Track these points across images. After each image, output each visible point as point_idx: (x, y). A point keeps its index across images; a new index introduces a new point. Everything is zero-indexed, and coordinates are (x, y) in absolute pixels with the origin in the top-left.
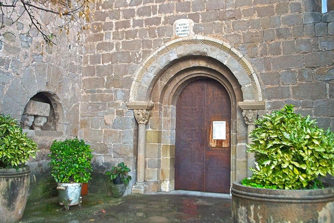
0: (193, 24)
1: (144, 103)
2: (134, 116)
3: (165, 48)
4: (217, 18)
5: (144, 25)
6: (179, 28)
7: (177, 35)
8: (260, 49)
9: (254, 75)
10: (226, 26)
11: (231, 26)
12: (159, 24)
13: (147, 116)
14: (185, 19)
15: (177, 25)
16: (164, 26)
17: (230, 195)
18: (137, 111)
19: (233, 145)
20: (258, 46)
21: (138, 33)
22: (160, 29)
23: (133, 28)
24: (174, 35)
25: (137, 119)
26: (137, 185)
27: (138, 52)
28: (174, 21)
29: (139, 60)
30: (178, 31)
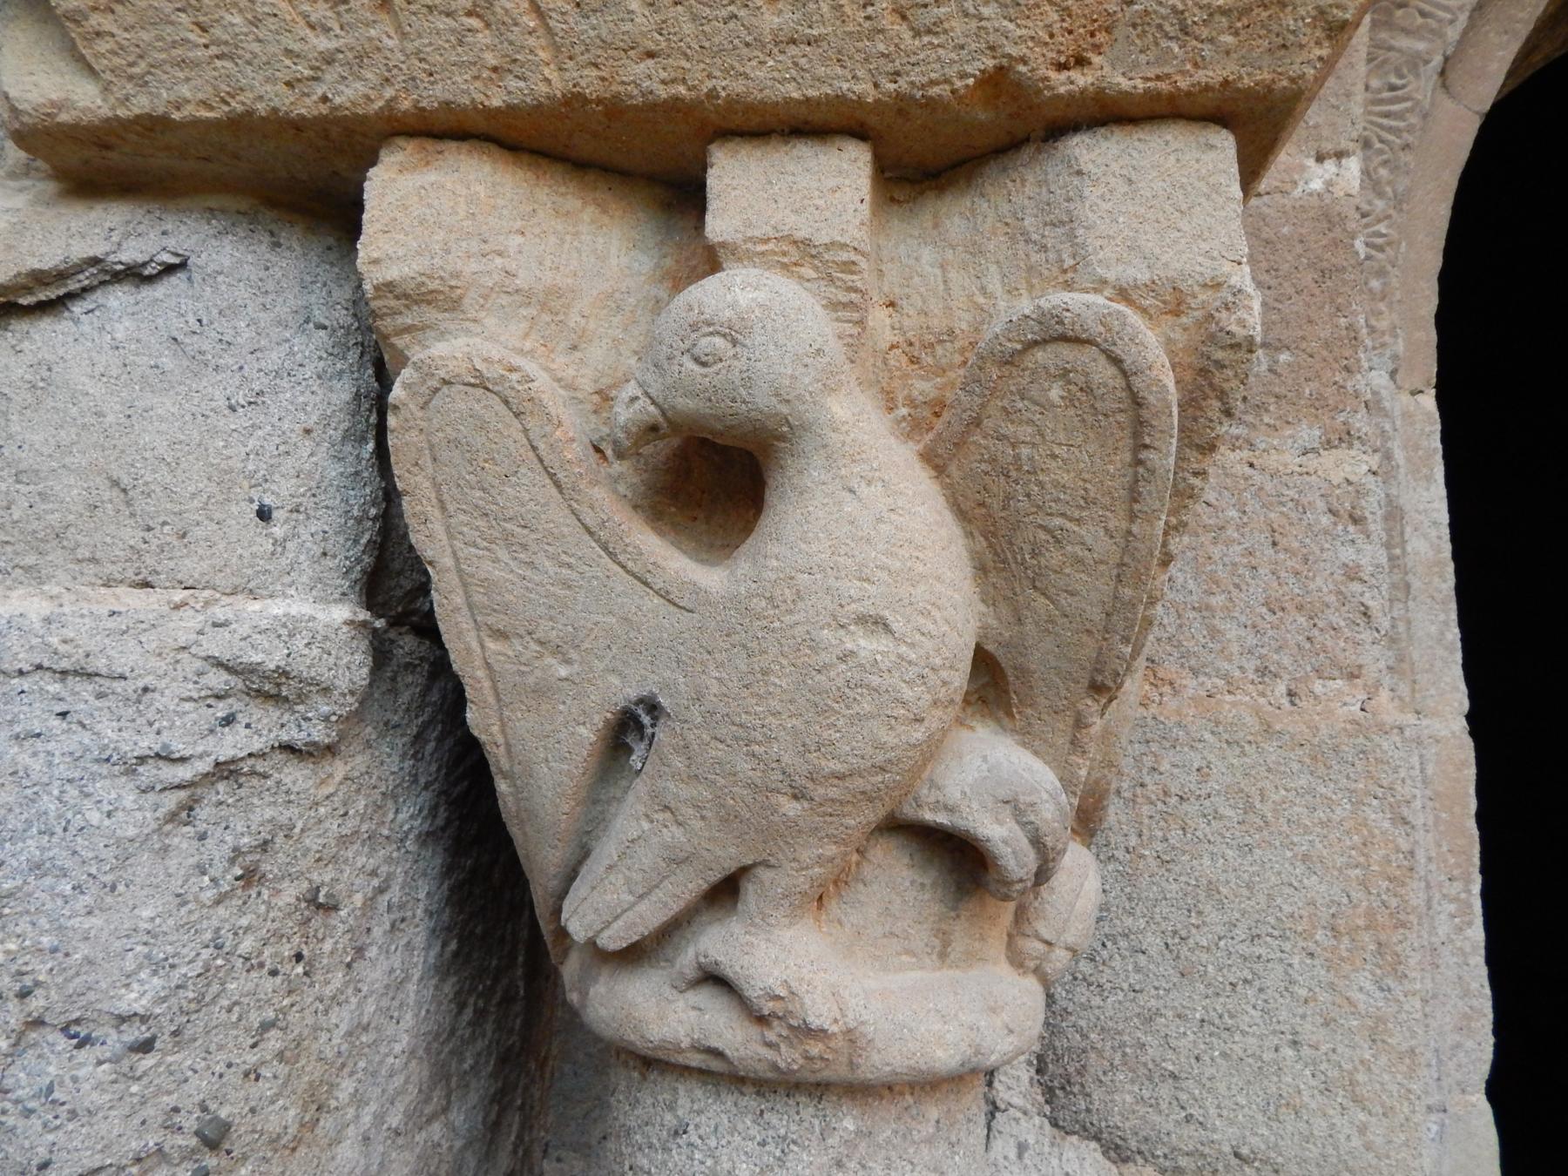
2: (393, 585)
25: (539, 752)
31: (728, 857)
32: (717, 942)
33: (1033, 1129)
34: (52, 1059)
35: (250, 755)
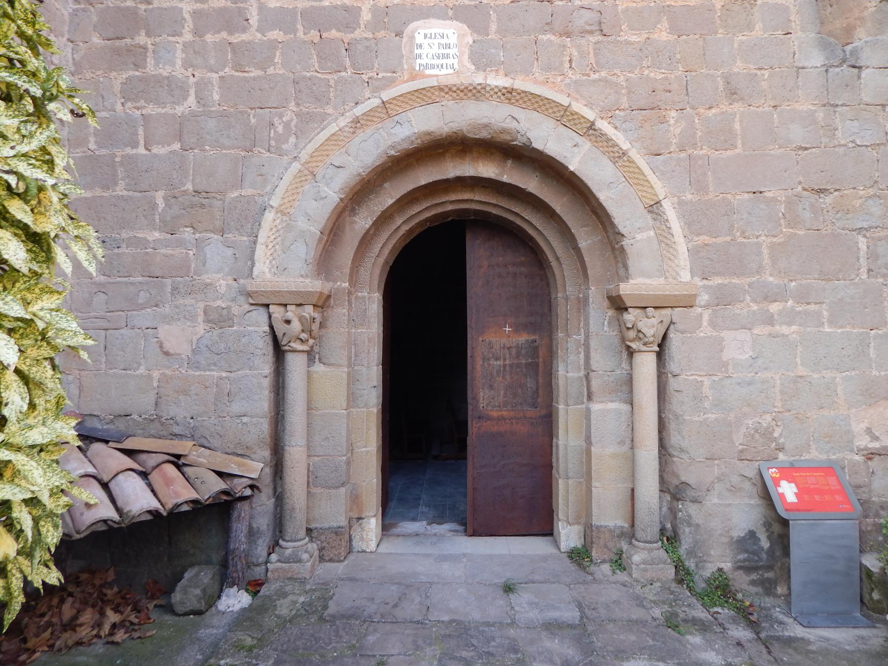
3: (378, 107)
4: (547, 28)
5: (299, 26)
6: (425, 46)
7: (417, 68)
8: (678, 131)
11: (592, 55)
12: (355, 29)
13: (315, 327)
15: (416, 34)
16: (371, 36)
18: (282, 309)
20: (672, 122)
21: (278, 54)
22: (359, 47)
23: (259, 36)
24: (406, 67)
25: (279, 335)
26: (288, 552)
27: (281, 116)
28: (406, 24)
29: (283, 143)
30: (420, 56)
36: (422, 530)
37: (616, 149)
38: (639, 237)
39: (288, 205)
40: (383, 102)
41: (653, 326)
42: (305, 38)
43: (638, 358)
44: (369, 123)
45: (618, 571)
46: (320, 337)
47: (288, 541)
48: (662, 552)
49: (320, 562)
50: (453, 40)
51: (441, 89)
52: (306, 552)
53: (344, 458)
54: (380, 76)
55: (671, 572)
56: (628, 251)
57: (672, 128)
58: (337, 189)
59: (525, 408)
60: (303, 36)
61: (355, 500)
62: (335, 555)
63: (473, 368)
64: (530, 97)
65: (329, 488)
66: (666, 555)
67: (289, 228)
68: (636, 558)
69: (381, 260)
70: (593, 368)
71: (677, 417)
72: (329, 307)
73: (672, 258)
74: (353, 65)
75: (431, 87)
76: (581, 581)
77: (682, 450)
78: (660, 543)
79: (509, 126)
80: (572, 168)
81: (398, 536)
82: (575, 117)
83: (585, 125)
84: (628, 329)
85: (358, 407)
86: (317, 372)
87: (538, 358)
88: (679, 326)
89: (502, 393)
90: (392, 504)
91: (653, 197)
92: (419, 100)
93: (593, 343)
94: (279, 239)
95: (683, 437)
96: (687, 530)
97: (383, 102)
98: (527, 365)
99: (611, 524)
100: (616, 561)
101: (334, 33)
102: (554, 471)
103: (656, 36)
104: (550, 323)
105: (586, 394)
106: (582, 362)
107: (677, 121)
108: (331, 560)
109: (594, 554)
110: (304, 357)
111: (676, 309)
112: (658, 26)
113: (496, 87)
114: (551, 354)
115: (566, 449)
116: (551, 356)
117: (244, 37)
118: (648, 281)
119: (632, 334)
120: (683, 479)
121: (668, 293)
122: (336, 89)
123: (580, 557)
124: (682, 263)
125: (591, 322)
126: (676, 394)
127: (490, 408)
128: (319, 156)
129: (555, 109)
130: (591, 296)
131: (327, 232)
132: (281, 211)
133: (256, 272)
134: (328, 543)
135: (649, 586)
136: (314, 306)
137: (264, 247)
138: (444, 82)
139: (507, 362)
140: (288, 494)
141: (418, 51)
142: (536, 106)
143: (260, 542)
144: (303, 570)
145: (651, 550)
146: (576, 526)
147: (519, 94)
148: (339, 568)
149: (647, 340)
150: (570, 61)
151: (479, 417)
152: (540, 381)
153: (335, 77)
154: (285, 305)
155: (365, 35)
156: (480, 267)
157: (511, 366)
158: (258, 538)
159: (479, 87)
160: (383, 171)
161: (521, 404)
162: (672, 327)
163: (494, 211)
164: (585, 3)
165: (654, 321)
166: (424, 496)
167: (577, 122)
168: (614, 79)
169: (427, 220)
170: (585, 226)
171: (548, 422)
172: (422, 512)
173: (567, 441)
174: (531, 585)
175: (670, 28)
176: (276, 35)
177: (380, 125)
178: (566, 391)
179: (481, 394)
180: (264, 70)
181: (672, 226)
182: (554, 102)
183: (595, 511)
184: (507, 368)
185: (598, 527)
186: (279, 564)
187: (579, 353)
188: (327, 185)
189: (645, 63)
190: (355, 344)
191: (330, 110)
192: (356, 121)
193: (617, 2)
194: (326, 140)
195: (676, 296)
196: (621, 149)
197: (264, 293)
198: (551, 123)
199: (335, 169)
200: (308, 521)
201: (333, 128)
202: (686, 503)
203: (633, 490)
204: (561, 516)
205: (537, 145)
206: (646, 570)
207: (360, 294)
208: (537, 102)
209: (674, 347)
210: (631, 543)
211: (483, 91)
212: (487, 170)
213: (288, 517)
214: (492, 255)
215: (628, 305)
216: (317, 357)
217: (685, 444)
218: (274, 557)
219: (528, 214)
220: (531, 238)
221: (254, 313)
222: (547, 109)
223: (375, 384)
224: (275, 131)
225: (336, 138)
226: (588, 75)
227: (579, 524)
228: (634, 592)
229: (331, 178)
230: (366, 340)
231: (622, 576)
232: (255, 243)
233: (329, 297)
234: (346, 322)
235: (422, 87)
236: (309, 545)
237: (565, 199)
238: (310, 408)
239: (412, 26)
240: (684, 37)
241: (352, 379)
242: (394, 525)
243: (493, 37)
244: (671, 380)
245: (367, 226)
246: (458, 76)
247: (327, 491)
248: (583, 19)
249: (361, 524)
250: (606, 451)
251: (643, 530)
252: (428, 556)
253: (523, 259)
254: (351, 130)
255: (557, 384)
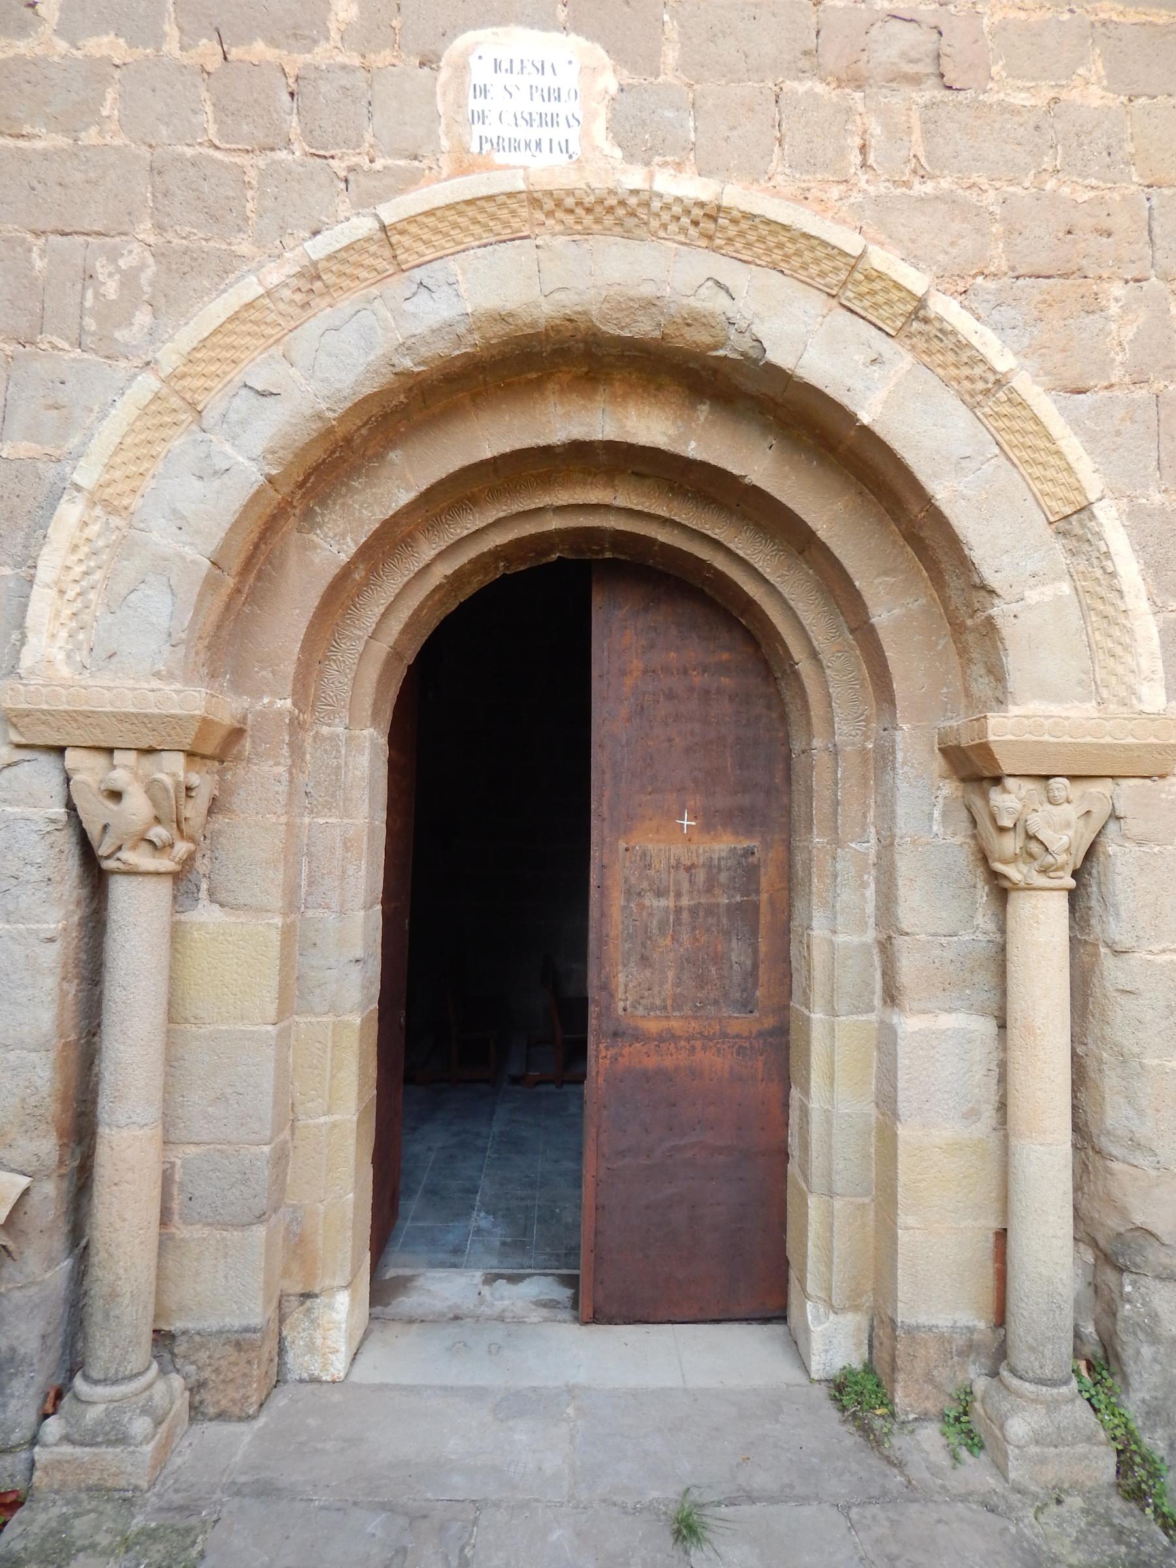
0: (609, 82)
1: (189, 699)
2: (70, 806)
3: (368, 239)
4: (804, 63)
5: (170, 29)
6: (496, 91)
7: (475, 148)
8: (1129, 333)
9: (1110, 520)
10: (876, 129)
11: (917, 135)
12: (315, 42)
13: (195, 811)
14: (545, 29)
15: (473, 60)
16: (357, 61)
17: (797, 1349)
18: (100, 760)
19: (833, 1013)
20: (1114, 309)
21: (110, 94)
22: (324, 87)
23: (62, 45)
24: (445, 143)
25: (93, 831)
26: (93, 1414)
27: (113, 256)
28: (446, 35)
29: (118, 326)
30: (482, 117)
31: (119, 843)
32: (119, 855)
33: (207, 902)
34: (29, 868)
35: (837, 803)
36: (468, 1304)
37: (978, 370)
38: (1033, 596)
39: (125, 487)
40: (383, 228)
41: (1068, 825)
42: (185, 59)
43: (1022, 907)
44: (345, 283)
45: (964, 1453)
46: (212, 837)
47: (96, 1382)
48: (1081, 1410)
49: (192, 1420)
50: (568, 79)
51: (534, 202)
52: (144, 1411)
53: (266, 1149)
54: (379, 165)
55: (1106, 1465)
56: (1005, 632)
57: (1114, 326)
58: (258, 451)
59: (726, 1012)
60: (177, 53)
61: (298, 1247)
62: (233, 1401)
63: (603, 915)
64: (764, 230)
65: (225, 1226)
66: (1092, 1419)
67: (125, 547)
68: (1018, 1427)
69: (382, 648)
70: (905, 926)
71: (1123, 1058)
72: (238, 758)
73: (1118, 650)
74: (308, 133)
75: (510, 195)
76: (875, 1492)
77: (1136, 1145)
78: (1074, 1384)
79: (709, 305)
80: (865, 418)
81: (411, 1321)
82: (877, 286)
83: (900, 308)
84: (1002, 830)
85: (311, 1011)
86: (202, 925)
87: (758, 892)
88: (1133, 826)
89: (671, 974)
90: (411, 1206)
91: (1071, 496)
92: (477, 230)
93: (905, 865)
94: (98, 576)
95: (1141, 1113)
96: (1147, 1351)
97: (383, 228)
98: (734, 910)
99: (943, 1320)
100: (957, 1419)
101: (260, 49)
102: (793, 1168)
103: (1075, 94)
104: (788, 810)
105: (878, 986)
106: (870, 908)
107: (1125, 309)
108: (222, 1416)
109: (899, 1398)
110: (164, 888)
111: (1124, 783)
112: (1081, 71)
113: (678, 200)
114: (790, 883)
115: (828, 1122)
116: (790, 890)
117: (23, 47)
118: (1055, 709)
119: (1011, 844)
120: (1139, 1219)
121: (1108, 740)
122: (263, 194)
123: (859, 1395)
124: (1145, 663)
125: (900, 811)
126: (1122, 999)
127: (641, 1011)
128: (211, 361)
129: (827, 266)
130: (900, 746)
131: (236, 565)
132: (102, 500)
133: (27, 660)
134: (217, 1371)
135: (1054, 1508)
136: (190, 754)
137: (53, 593)
138: (544, 183)
139: (685, 901)
140: (103, 1255)
141: (475, 104)
142: (777, 255)
143: (17, 1386)
144: (131, 1464)
145: (1053, 1406)
146: (850, 1316)
147: (734, 221)
148: (236, 1444)
149: (1050, 859)
150: (863, 149)
151: (615, 1034)
152: (763, 948)
153: (261, 161)
154: (110, 751)
155: (341, 59)
156: (624, 673)
157: (693, 911)
158: (12, 1376)
159: (633, 201)
160: (385, 416)
161: (716, 1002)
162: (1113, 827)
163: (663, 536)
164: (902, 6)
165: (1071, 812)
166: (484, 1183)
167: (880, 299)
168: (972, 196)
169: (497, 554)
170: (886, 573)
171: (779, 1050)
172: (479, 1231)
173: (831, 1101)
174: (746, 1509)
175: (1108, 77)
176: (106, 45)
177: (375, 291)
178: (831, 977)
179: (621, 978)
180: (73, 133)
181: (1121, 570)
182: (824, 244)
183: (904, 1287)
184: (685, 916)
185: (911, 1331)
186: (67, 1449)
187: (864, 885)
188: (233, 438)
189: (1047, 162)
190: (309, 854)
191: (244, 247)
192: (312, 273)
193: (980, 8)
194: (231, 320)
195: (1127, 748)
196: (992, 370)
197: (48, 717)
198: (817, 301)
199: (254, 400)
200: (157, 1317)
201: (248, 288)
202: (1144, 1281)
203: (1002, 1236)
204: (811, 1287)
205: (779, 356)
206: (1043, 1461)
207: (325, 730)
208: (780, 246)
209: (1119, 879)
210: (994, 1374)
211: (642, 212)
212: (649, 425)
213: (98, 1317)
214: (652, 646)
215: (1006, 769)
216: (204, 886)
217: (1145, 1130)
218: (53, 1427)
219: (743, 544)
220: (750, 604)
221: (23, 771)
222: (805, 267)
223: (359, 953)
224: (97, 295)
225: (255, 315)
226: (907, 184)
227: (856, 1308)
228: (1021, 1536)
229: (243, 423)
230: (339, 845)
231: (975, 1473)
232: (31, 582)
233: (237, 733)
234: (283, 798)
235: (484, 191)
236: (160, 1387)
237: (840, 505)
238: (174, 1013)
239: (461, 42)
240: (1143, 100)
241: (295, 943)
242: (402, 1284)
243: (670, 78)
244: (1108, 962)
245: (344, 558)
246: (580, 169)
247: (218, 1234)
248: (896, 45)
249: (309, 1311)
250: (937, 1135)
251: (1032, 1349)
252: (477, 1394)
253: (725, 656)
254: (298, 297)
255: (808, 960)
